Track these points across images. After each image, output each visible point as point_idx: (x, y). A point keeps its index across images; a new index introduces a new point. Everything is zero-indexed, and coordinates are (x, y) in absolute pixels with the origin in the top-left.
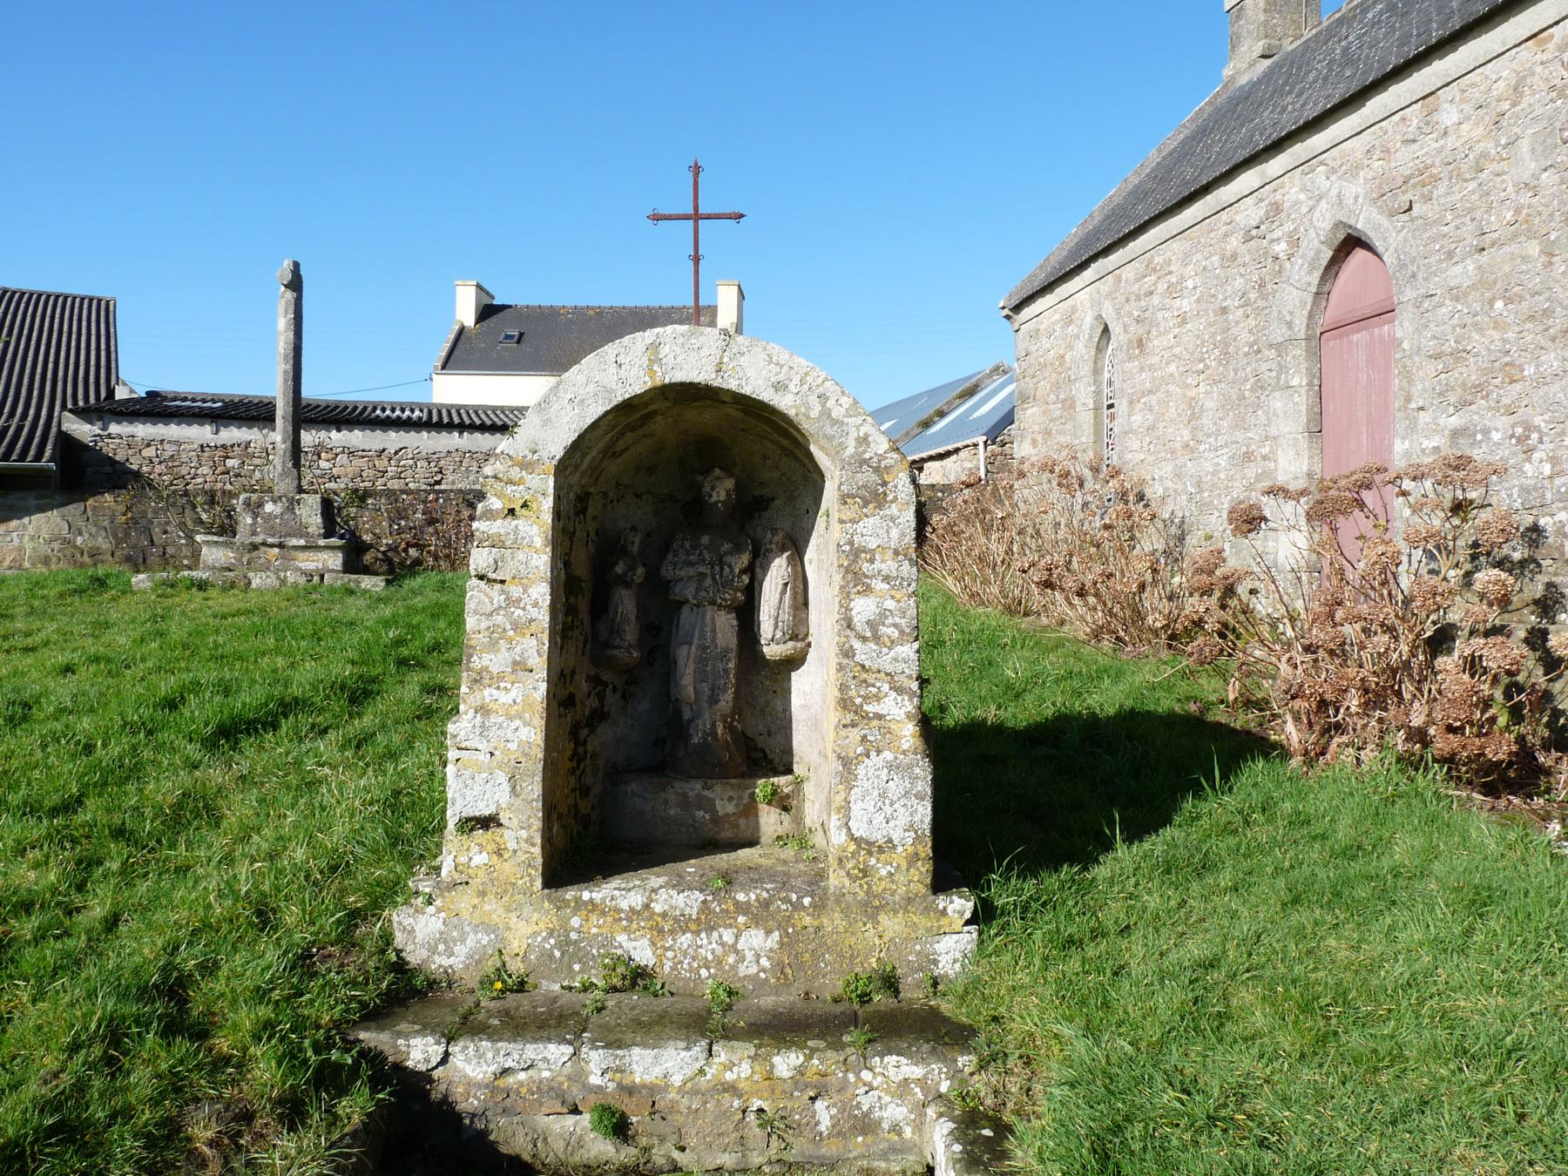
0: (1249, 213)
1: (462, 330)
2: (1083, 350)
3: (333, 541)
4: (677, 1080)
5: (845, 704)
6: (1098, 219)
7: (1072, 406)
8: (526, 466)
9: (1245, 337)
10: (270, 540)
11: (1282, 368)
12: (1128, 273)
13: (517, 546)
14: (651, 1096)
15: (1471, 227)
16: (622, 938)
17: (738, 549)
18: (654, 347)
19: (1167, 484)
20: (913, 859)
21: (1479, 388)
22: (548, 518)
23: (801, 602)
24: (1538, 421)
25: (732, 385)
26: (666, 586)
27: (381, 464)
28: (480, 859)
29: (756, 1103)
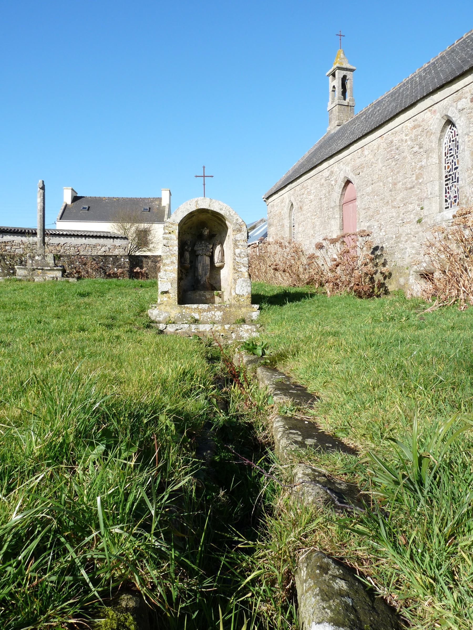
0: (326, 173)
1: (66, 205)
2: (286, 210)
3: (59, 268)
4: (208, 330)
5: (234, 269)
6: (291, 172)
7: (283, 226)
8: (172, 224)
9: (326, 206)
10: (39, 268)
11: (334, 213)
12: (297, 188)
13: (171, 239)
14: (203, 333)
15: (370, 179)
16: (193, 314)
17: (210, 244)
18: (197, 201)
19: (309, 247)
20: (248, 298)
21: (372, 216)
22: (177, 234)
23: (223, 255)
24: (382, 223)
25: (212, 209)
26: (195, 252)
27: (58, 248)
28: (165, 299)
29: (222, 334)
